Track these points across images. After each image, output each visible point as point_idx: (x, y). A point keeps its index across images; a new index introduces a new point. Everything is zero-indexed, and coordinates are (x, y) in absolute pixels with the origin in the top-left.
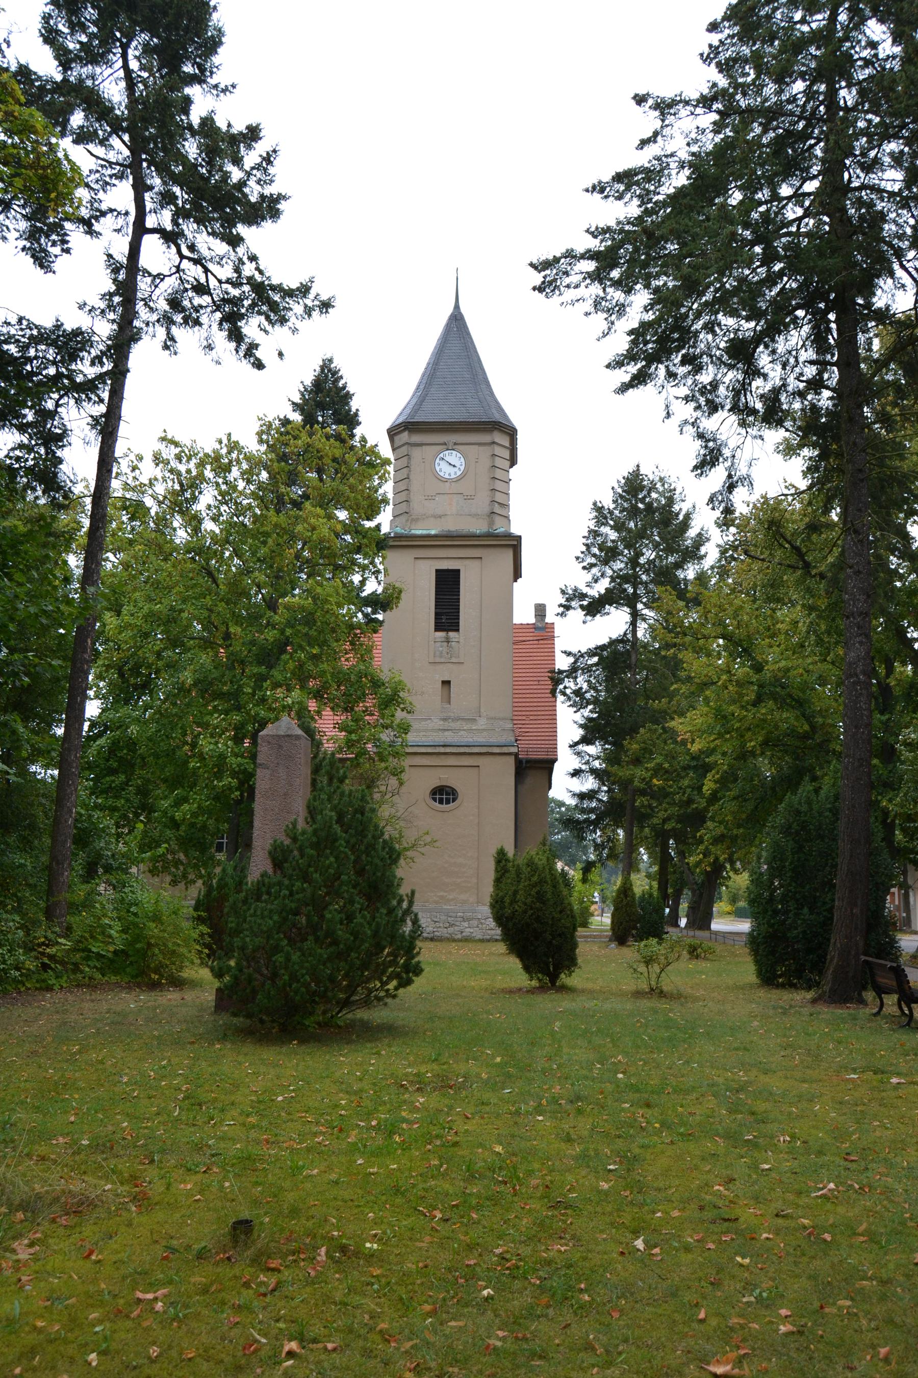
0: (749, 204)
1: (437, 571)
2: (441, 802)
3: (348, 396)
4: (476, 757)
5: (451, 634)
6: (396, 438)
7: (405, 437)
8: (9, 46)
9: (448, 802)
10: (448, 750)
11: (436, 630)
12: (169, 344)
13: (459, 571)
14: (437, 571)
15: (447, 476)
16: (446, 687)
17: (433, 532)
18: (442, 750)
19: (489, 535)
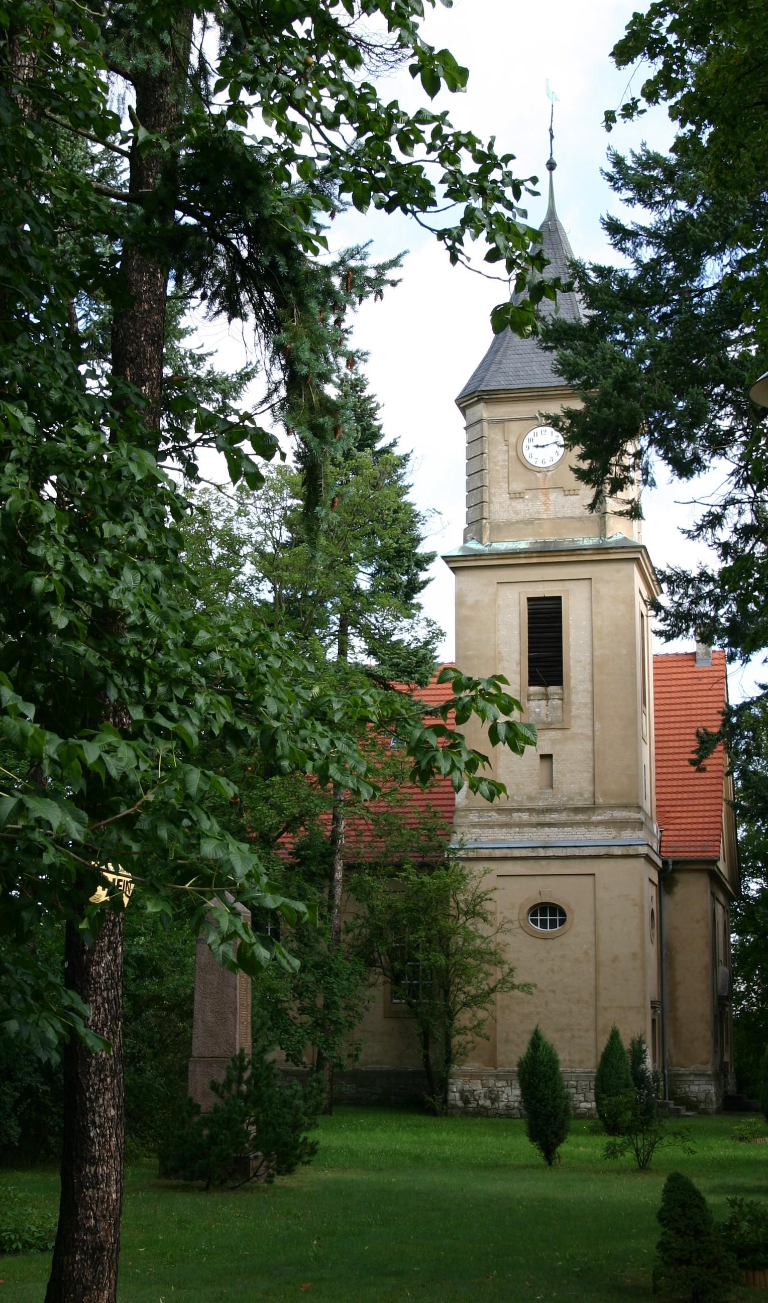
0: (762, 264)
1: (529, 599)
2: (543, 924)
3: (649, 81)
4: (588, 862)
5: (552, 689)
6: (468, 412)
7: (482, 411)
8: (458, 78)
9: (553, 926)
10: (550, 852)
11: (531, 684)
12: (508, 158)
13: (560, 598)
14: (529, 599)
15: (539, 464)
16: (546, 763)
17: (523, 545)
18: (542, 852)
19: (598, 549)
